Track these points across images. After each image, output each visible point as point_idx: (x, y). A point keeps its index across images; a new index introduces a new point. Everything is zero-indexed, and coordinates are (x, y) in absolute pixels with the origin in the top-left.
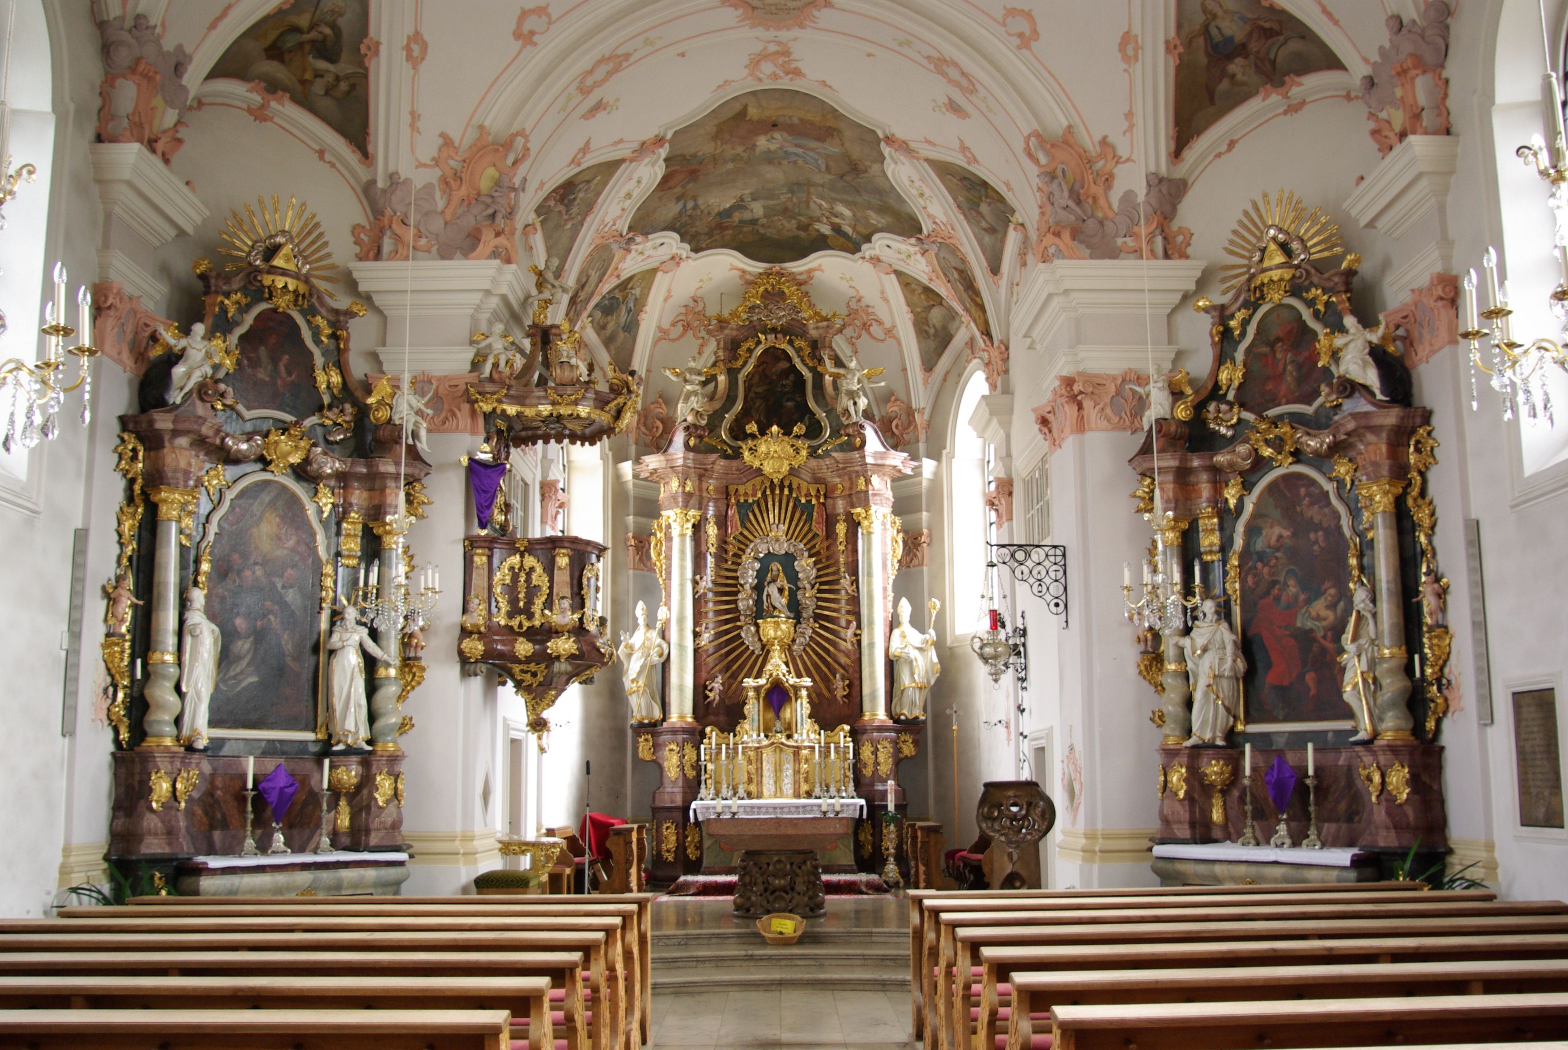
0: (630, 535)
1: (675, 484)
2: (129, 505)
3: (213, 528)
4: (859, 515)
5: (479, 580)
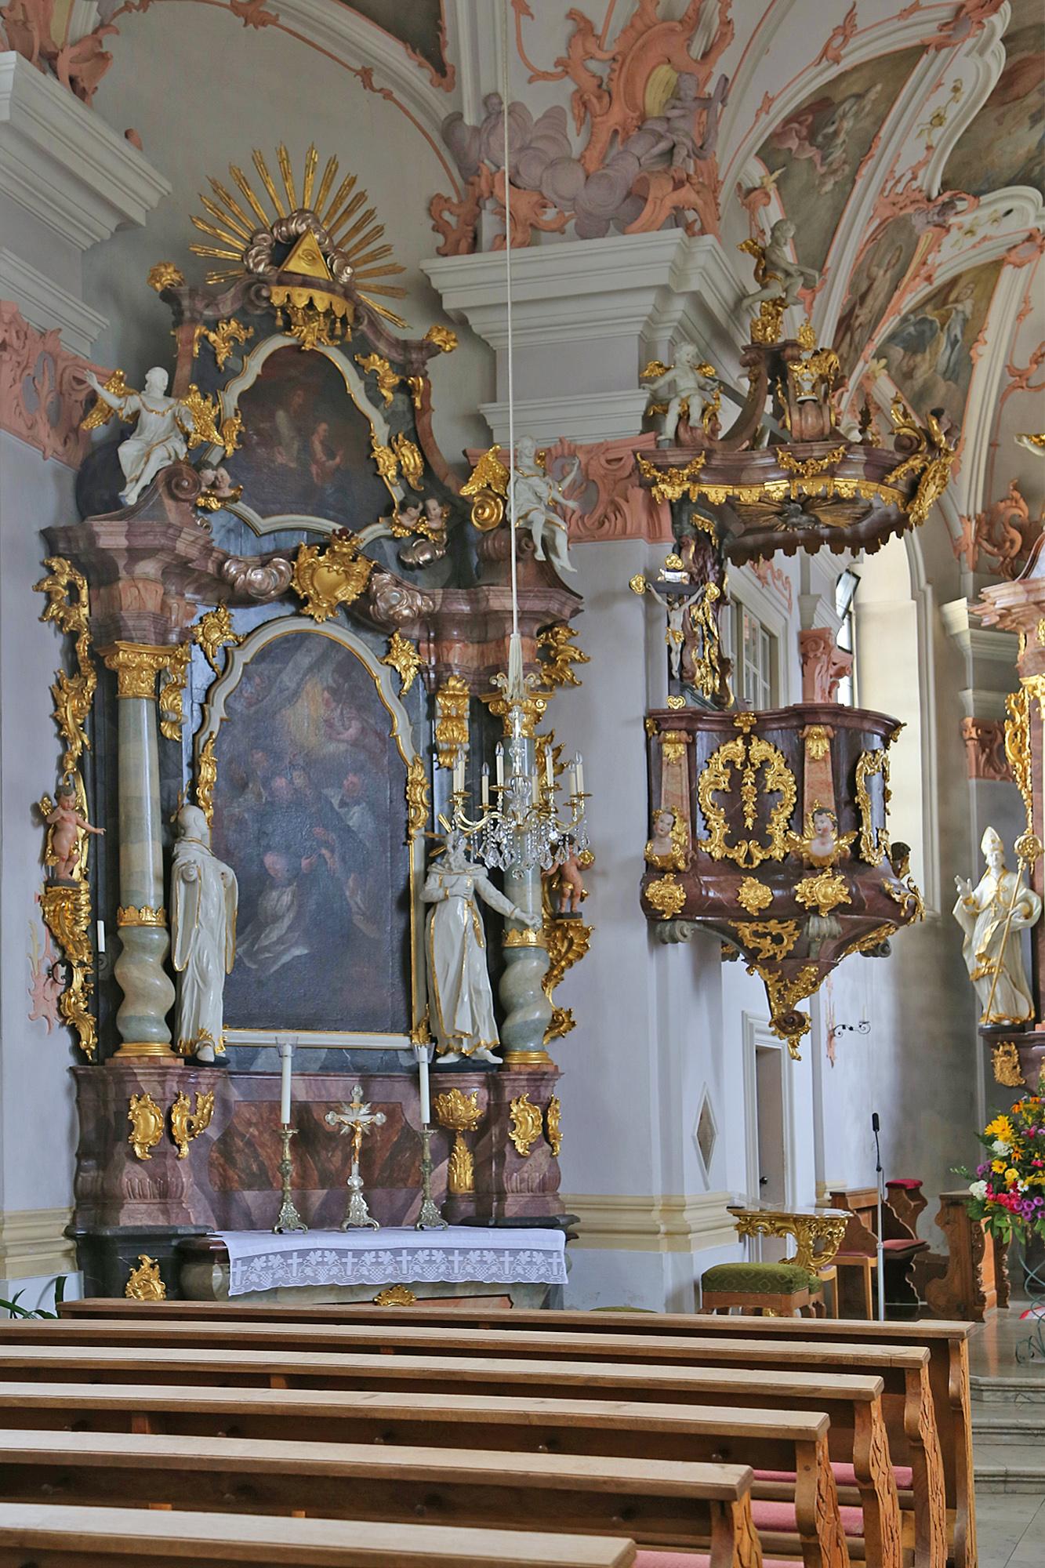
0: (969, 721)
2: (71, 677)
3: (217, 712)
5: (674, 784)
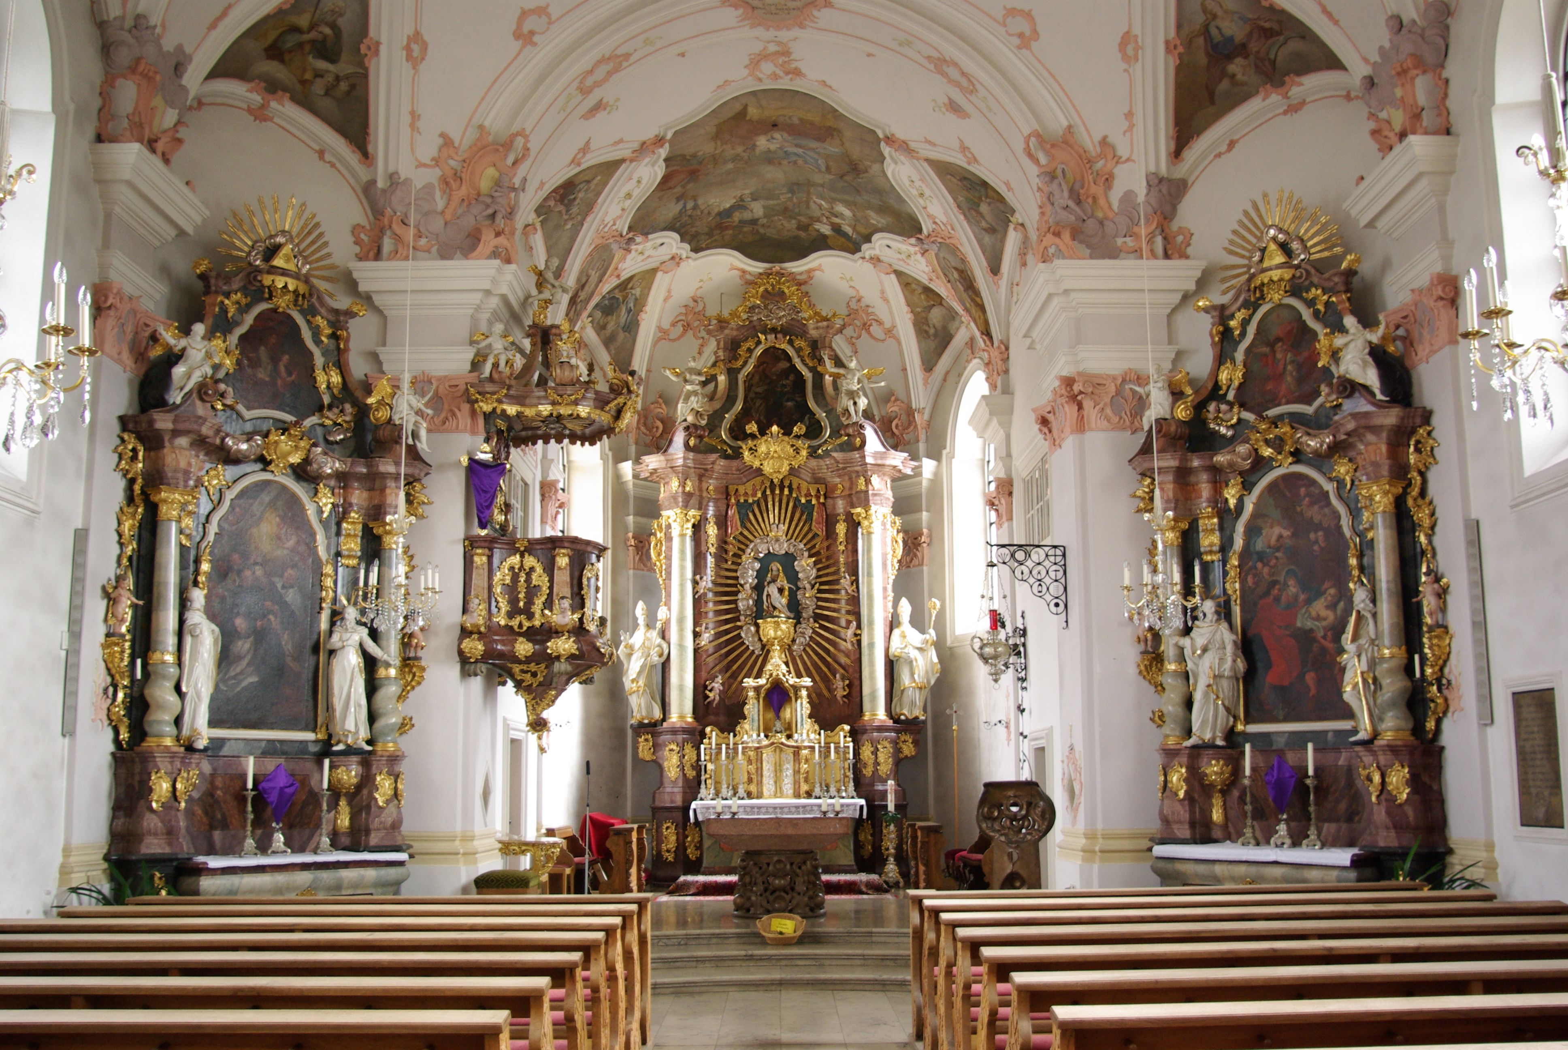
0: (630, 535)
1: (675, 484)
2: (129, 505)
3: (213, 528)
4: (859, 515)
5: (479, 580)
